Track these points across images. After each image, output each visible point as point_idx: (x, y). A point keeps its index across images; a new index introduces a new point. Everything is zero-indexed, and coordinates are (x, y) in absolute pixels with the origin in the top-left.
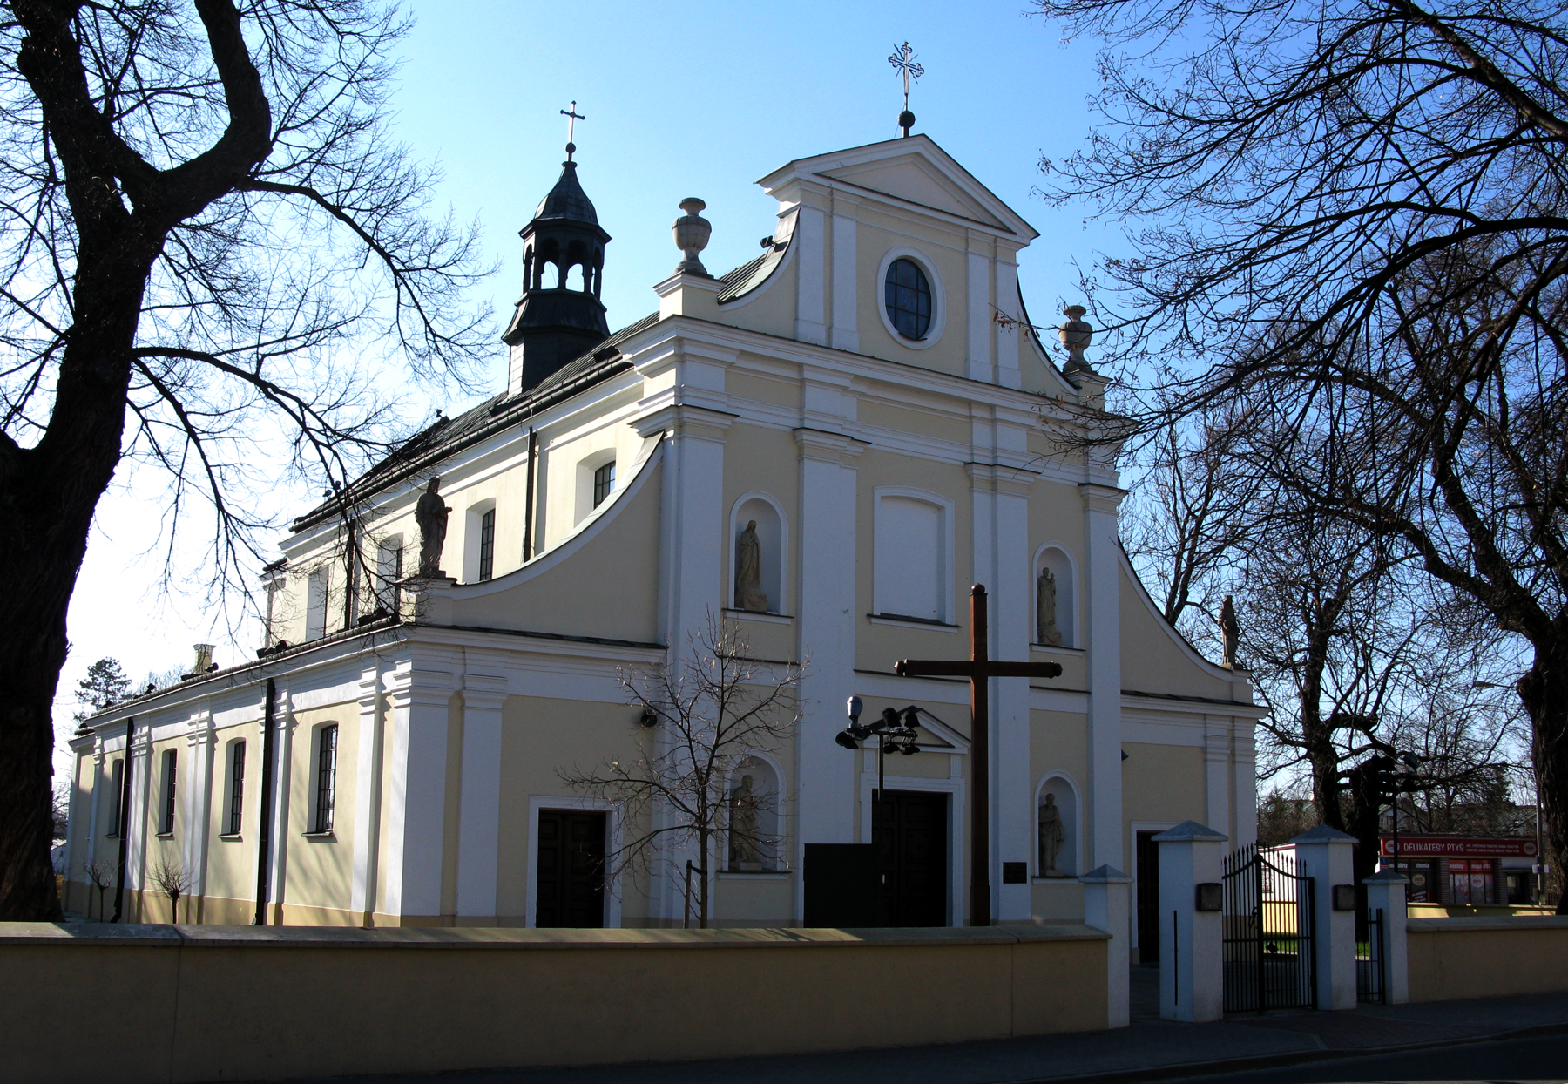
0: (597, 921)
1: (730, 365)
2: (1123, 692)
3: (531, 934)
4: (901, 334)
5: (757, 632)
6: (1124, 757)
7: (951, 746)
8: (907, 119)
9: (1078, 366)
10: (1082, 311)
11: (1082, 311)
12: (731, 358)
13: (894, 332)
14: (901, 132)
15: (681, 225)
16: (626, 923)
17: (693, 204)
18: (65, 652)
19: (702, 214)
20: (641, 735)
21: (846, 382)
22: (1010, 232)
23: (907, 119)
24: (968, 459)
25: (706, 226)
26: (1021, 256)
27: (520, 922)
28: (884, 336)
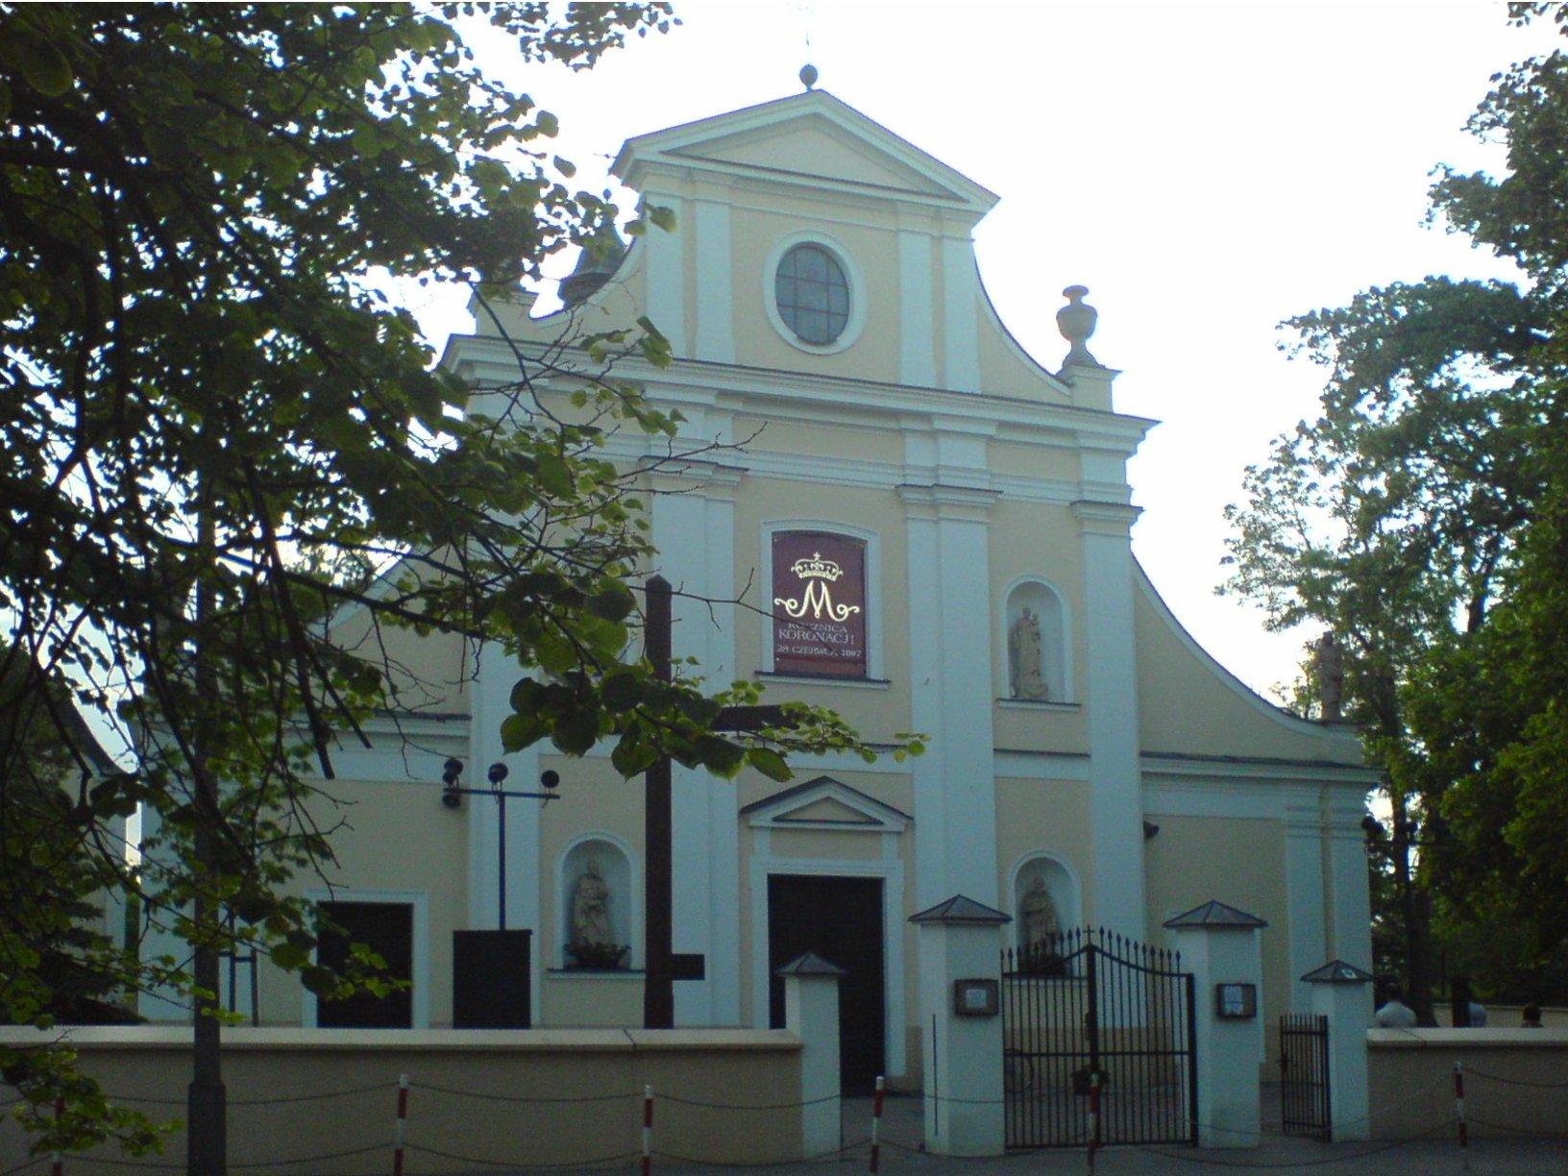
0: (523, 1022)
1: (990, 438)
2: (1085, 756)
3: (314, 1035)
4: (801, 338)
5: (1033, 727)
6: (1150, 831)
7: (880, 823)
8: (808, 75)
9: (1079, 360)
10: (1083, 291)
11: (1083, 291)
12: (991, 431)
13: (789, 336)
14: (803, 89)
15: (1063, 317)
16: (434, 1025)
17: (1075, 292)
18: (621, 771)
19: (1086, 300)
20: (448, 817)
21: (710, 399)
22: (960, 199)
23: (808, 75)
24: (1074, 497)
25: (1091, 314)
26: (980, 232)
27: (298, 1024)
28: (777, 344)
